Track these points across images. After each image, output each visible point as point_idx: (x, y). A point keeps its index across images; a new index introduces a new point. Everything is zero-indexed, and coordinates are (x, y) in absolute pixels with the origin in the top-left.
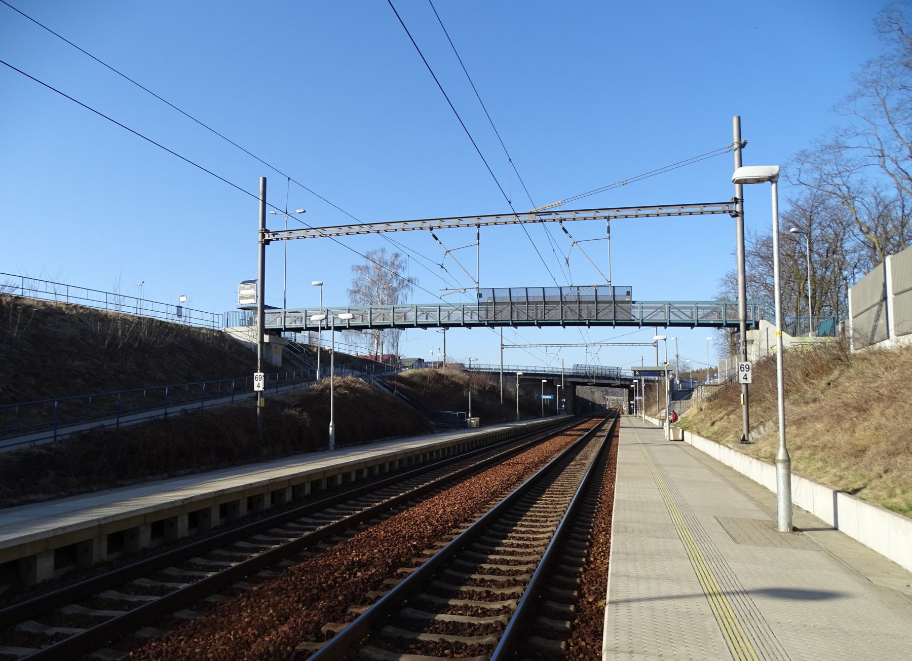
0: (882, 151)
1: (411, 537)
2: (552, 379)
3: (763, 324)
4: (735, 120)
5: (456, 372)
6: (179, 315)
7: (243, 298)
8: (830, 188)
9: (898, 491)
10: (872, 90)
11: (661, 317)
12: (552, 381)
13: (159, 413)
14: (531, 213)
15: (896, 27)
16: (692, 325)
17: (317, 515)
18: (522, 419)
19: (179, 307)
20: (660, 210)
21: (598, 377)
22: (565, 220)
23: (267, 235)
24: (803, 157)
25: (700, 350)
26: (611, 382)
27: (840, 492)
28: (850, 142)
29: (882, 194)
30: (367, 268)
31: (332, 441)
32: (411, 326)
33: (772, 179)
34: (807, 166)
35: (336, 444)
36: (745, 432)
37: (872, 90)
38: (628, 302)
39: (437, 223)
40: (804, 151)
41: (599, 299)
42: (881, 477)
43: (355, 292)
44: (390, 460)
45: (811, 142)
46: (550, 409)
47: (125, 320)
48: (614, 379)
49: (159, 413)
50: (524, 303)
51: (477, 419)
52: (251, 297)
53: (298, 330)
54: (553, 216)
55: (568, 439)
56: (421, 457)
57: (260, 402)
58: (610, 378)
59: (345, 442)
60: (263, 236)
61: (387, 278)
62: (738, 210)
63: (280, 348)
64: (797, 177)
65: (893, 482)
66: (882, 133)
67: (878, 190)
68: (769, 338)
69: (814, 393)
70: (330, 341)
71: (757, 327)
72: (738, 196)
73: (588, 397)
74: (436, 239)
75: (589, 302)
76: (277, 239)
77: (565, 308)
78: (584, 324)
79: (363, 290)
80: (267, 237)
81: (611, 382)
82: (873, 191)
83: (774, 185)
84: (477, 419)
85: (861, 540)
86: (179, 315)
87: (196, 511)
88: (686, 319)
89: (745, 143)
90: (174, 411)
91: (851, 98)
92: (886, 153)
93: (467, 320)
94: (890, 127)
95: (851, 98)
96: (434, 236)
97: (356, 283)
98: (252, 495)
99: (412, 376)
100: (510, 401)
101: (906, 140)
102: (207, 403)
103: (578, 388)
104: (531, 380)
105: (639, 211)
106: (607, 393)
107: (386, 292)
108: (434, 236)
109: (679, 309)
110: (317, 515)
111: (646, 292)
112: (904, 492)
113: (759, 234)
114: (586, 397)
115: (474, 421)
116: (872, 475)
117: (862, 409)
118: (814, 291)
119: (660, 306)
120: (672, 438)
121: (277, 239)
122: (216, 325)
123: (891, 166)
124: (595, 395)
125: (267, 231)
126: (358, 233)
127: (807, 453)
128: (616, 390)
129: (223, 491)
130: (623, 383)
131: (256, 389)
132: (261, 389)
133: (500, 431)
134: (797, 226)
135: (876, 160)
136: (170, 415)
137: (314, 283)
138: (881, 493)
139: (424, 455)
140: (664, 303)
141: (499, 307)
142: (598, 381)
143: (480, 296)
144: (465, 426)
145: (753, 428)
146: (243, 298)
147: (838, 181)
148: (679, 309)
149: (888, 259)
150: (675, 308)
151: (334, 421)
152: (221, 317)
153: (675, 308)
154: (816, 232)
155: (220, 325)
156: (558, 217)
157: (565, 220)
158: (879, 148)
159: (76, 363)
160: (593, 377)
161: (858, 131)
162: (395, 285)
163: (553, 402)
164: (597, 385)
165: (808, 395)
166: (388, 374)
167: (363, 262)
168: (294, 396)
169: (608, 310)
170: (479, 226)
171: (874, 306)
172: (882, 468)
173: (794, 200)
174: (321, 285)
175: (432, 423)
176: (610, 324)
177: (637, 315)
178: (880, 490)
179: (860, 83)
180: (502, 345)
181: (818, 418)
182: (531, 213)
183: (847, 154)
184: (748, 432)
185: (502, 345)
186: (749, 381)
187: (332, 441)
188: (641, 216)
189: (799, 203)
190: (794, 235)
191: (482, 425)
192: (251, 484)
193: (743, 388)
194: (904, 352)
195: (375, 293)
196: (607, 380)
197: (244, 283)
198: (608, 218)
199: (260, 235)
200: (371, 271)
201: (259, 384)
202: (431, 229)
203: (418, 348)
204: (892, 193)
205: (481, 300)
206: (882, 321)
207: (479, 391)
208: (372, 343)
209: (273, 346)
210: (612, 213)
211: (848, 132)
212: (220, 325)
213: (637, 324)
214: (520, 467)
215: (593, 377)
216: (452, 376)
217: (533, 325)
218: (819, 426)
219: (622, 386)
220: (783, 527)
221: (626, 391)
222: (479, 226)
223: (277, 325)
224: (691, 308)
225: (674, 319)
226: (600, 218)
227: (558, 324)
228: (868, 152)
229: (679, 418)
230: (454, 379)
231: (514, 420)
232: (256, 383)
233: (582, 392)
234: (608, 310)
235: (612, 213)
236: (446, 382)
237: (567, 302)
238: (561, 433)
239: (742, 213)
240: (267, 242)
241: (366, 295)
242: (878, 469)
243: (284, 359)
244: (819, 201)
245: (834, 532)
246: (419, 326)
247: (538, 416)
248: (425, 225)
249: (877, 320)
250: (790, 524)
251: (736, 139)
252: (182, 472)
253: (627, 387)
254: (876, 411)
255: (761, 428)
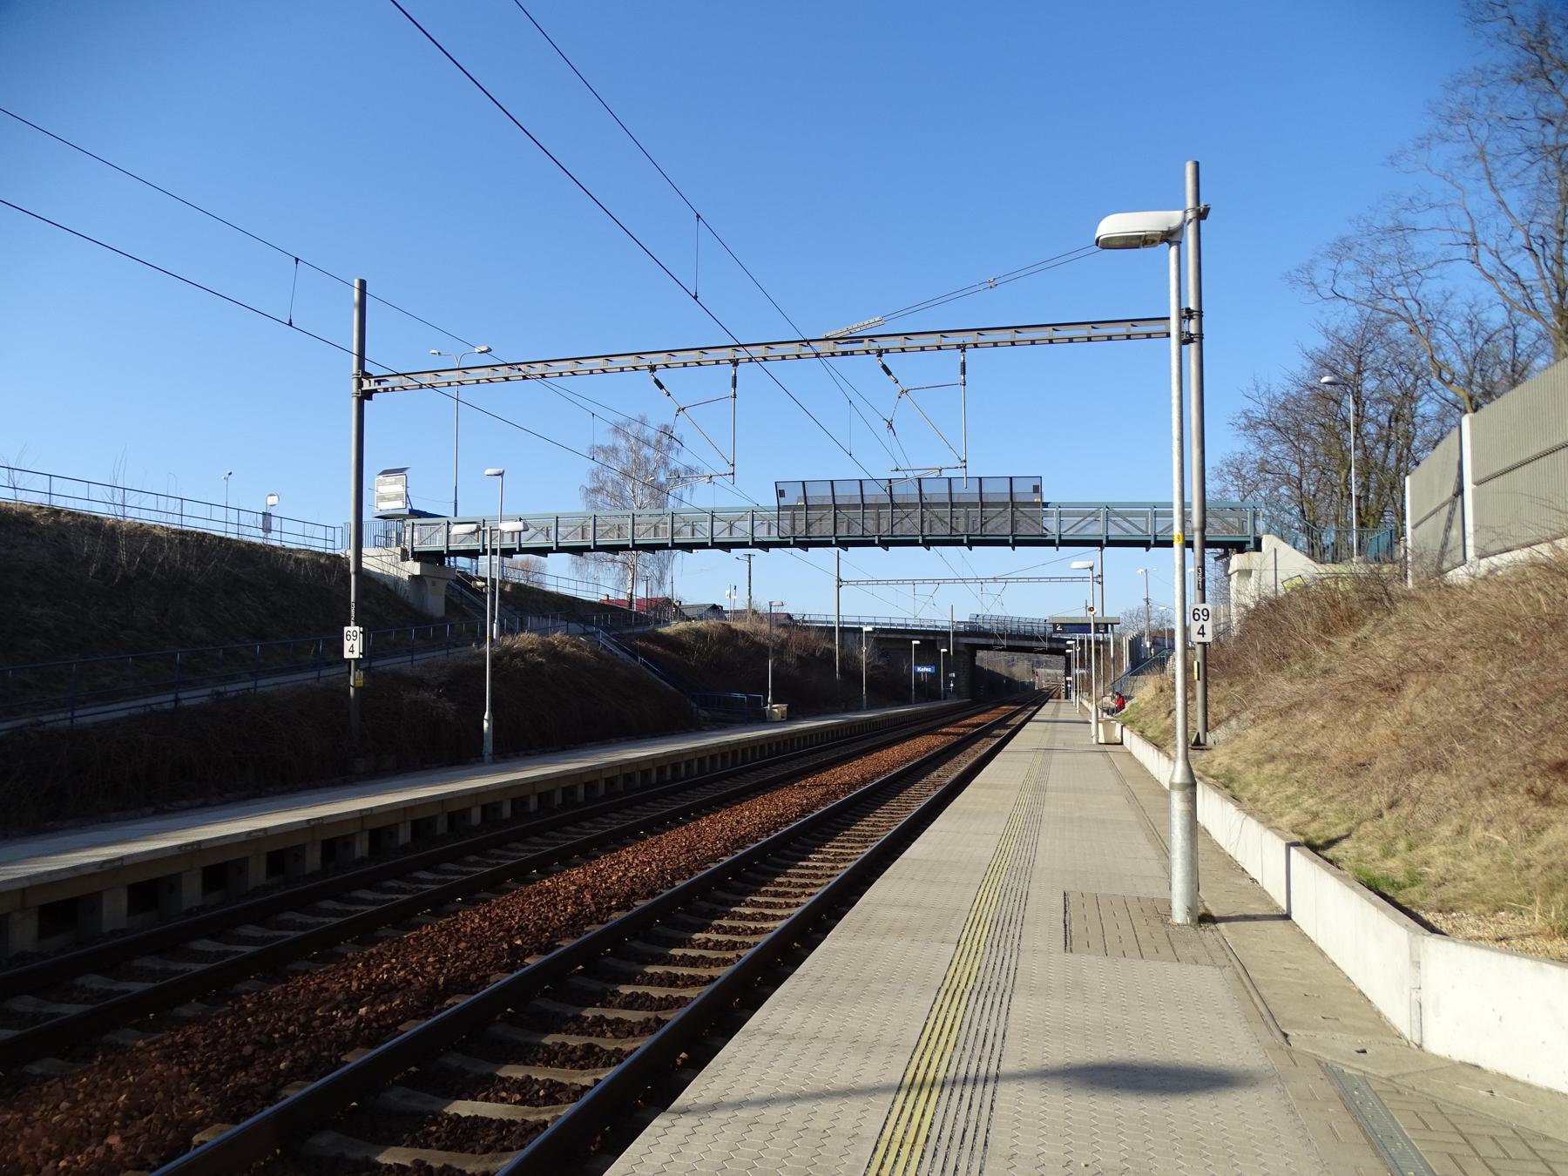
0: (1473, 235)
1: (522, 929)
2: (931, 640)
3: (1268, 541)
4: (1189, 168)
5: (765, 627)
6: (267, 529)
7: (383, 498)
8: (1394, 306)
9: (1401, 845)
10: (1462, 129)
11: (1095, 530)
12: (934, 642)
13: (165, 700)
14: (827, 339)
15: (1504, 12)
16: (1146, 544)
17: (390, 884)
18: (871, 707)
19: (267, 516)
20: (1055, 332)
21: (1011, 636)
22: (887, 351)
23: (366, 382)
24: (1342, 249)
25: (1144, 589)
26: (1034, 644)
27: (1296, 844)
28: (1424, 220)
29: (1484, 316)
30: (615, 450)
31: (488, 746)
32: (703, 546)
33: (1170, 237)
34: (1348, 266)
35: (494, 754)
36: (1200, 730)
37: (1462, 129)
38: (1036, 505)
39: (663, 358)
40: (1343, 240)
41: (1017, 499)
42: (1381, 816)
43: (596, 491)
44: (605, 775)
45: (1350, 221)
46: (928, 690)
47: (141, 534)
48: (1038, 639)
49: (165, 700)
50: (856, 506)
51: (784, 707)
52: (397, 497)
53: (473, 554)
54: (866, 344)
55: (942, 739)
56: (654, 774)
57: (355, 679)
58: (1032, 637)
59: (511, 748)
60: (360, 384)
61: (648, 465)
62: (1193, 331)
63: (442, 586)
64: (1330, 285)
65: (1396, 827)
66: (1473, 204)
67: (1475, 310)
68: (1282, 564)
69: (1328, 661)
70: (559, 576)
71: (1258, 548)
72: (1192, 306)
73: (1001, 669)
74: (661, 387)
75: (968, 505)
76: (386, 390)
77: (927, 514)
78: (959, 543)
79: (609, 487)
80: (366, 386)
81: (1034, 644)
82: (1466, 310)
83: (1173, 250)
84: (784, 707)
85: (1321, 944)
86: (267, 529)
87: (148, 885)
88: (1137, 534)
89: (1207, 210)
90: (194, 697)
91: (1423, 143)
92: (1480, 238)
93: (762, 534)
94: (1491, 196)
95: (1423, 143)
96: (657, 381)
97: (595, 475)
98: (279, 851)
99: (680, 633)
100: (851, 672)
101: (1519, 219)
102: (266, 684)
103: (980, 654)
104: (892, 641)
105: (1017, 334)
106: (1039, 664)
107: (647, 491)
108: (657, 381)
109: (1123, 516)
110: (390, 884)
111: (1068, 487)
112: (1410, 847)
113: (1278, 391)
114: (998, 670)
115: (778, 709)
116: (1369, 810)
117: (1390, 688)
118: (1365, 487)
119: (1090, 512)
120: (1102, 740)
121: (386, 390)
122: (330, 544)
123: (1487, 260)
124: (1019, 668)
125: (368, 376)
126: (507, 379)
127: (1282, 768)
128: (1044, 657)
129: (199, 843)
130: (1054, 645)
131: (347, 655)
132: (356, 655)
133: (818, 728)
134: (1334, 372)
135: (1462, 252)
136: (185, 703)
137: (488, 471)
138: (1369, 849)
139: (661, 770)
140: (1098, 506)
141: (814, 514)
142: (1011, 643)
143: (781, 494)
144: (763, 719)
145: (1219, 723)
146: (383, 498)
147: (1402, 292)
148: (1123, 516)
149: (1466, 421)
150: (1118, 514)
151: (492, 710)
152: (338, 531)
153: (1118, 514)
154: (1370, 385)
155: (338, 544)
156: (874, 346)
157: (887, 351)
158: (1468, 228)
159: (37, 611)
160: (1002, 636)
161: (1434, 200)
162: (662, 479)
163: (934, 677)
164: (1010, 649)
165: (1321, 664)
166: (638, 630)
167: (607, 440)
168: (442, 667)
169: (1004, 520)
170: (735, 363)
171: (1443, 505)
172: (1385, 799)
173: (1332, 328)
174: (501, 474)
175: (706, 714)
176: (1004, 543)
177: (1051, 526)
178: (1370, 843)
179: (1440, 117)
180: (839, 580)
181: (1314, 704)
182: (827, 339)
183: (1419, 244)
184: (1206, 730)
185: (839, 580)
186: (1209, 638)
187: (488, 746)
188: (1022, 343)
189: (1343, 334)
190: (1328, 387)
191: (791, 716)
192: (265, 830)
193: (1199, 649)
194: (1479, 583)
195: (628, 493)
196: (1022, 641)
197: (385, 473)
198: (962, 347)
199: (355, 381)
200: (622, 455)
201: (353, 644)
202: (653, 369)
203: (703, 584)
204: (1497, 317)
205: (783, 502)
206: (1455, 532)
207: (799, 658)
208: (625, 578)
209: (428, 581)
210: (970, 338)
211: (1417, 203)
212: (338, 544)
213: (1051, 543)
214: (820, 790)
215: (1002, 636)
216: (756, 634)
217: (871, 544)
218: (1315, 718)
219: (1051, 651)
220: (1179, 915)
221: (1062, 659)
222: (735, 363)
223: (438, 544)
224: (1144, 514)
225: (1115, 533)
226: (948, 347)
227: (914, 543)
228: (1448, 237)
229: (1127, 705)
230: (757, 639)
231: (858, 709)
232: (347, 645)
233: (984, 658)
234: (1004, 520)
235: (970, 338)
236: (741, 643)
237: (932, 505)
238: (930, 731)
239: (1201, 336)
240: (368, 395)
241: (613, 496)
242: (1379, 800)
243: (450, 604)
244: (1373, 331)
245: (1280, 923)
246: (716, 545)
247: (906, 701)
248: (642, 362)
249: (1448, 528)
250: (1191, 910)
251: (1190, 203)
252: (185, 803)
253: (1061, 652)
254: (1411, 690)
255: (1233, 722)
